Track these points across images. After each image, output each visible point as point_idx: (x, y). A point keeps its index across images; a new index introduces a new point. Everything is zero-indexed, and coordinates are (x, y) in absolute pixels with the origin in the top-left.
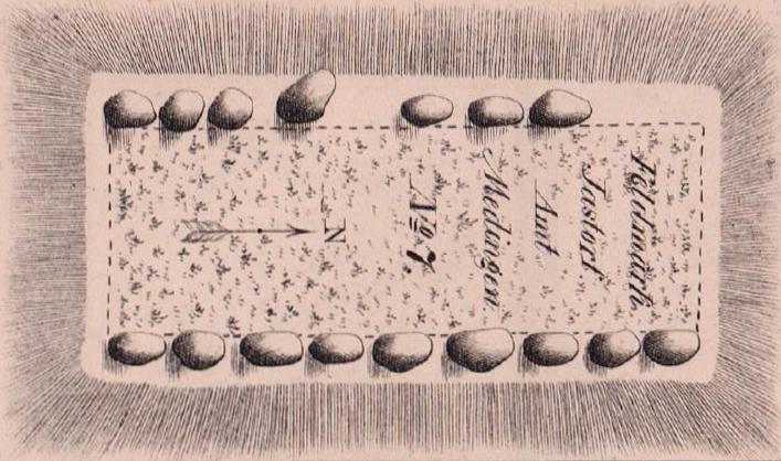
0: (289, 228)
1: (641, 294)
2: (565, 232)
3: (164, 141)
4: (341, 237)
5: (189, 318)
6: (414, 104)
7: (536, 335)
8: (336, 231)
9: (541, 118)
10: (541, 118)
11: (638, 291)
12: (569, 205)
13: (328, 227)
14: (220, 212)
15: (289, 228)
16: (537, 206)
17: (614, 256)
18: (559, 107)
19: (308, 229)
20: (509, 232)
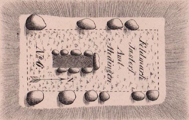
0: (60, 79)
1: (142, 76)
2: (125, 59)
3: (100, 102)
4: (72, 80)
5: (95, 50)
6: (63, 51)
7: (63, 91)
8: (71, 79)
9: (128, 27)
10: (128, 27)
11: (141, 76)
12: (126, 52)
13: (72, 82)
14: (104, 76)
15: (60, 79)
16: (118, 53)
17: (136, 67)
18: (133, 23)
19: (65, 78)
20: (113, 62)
